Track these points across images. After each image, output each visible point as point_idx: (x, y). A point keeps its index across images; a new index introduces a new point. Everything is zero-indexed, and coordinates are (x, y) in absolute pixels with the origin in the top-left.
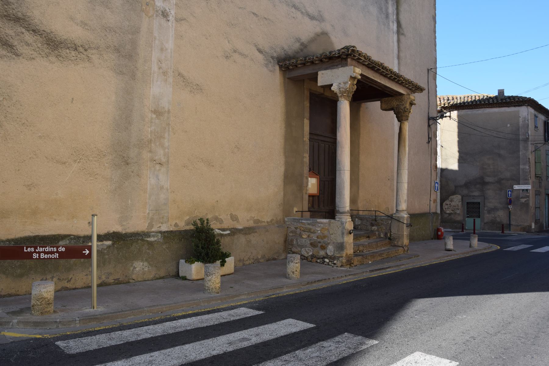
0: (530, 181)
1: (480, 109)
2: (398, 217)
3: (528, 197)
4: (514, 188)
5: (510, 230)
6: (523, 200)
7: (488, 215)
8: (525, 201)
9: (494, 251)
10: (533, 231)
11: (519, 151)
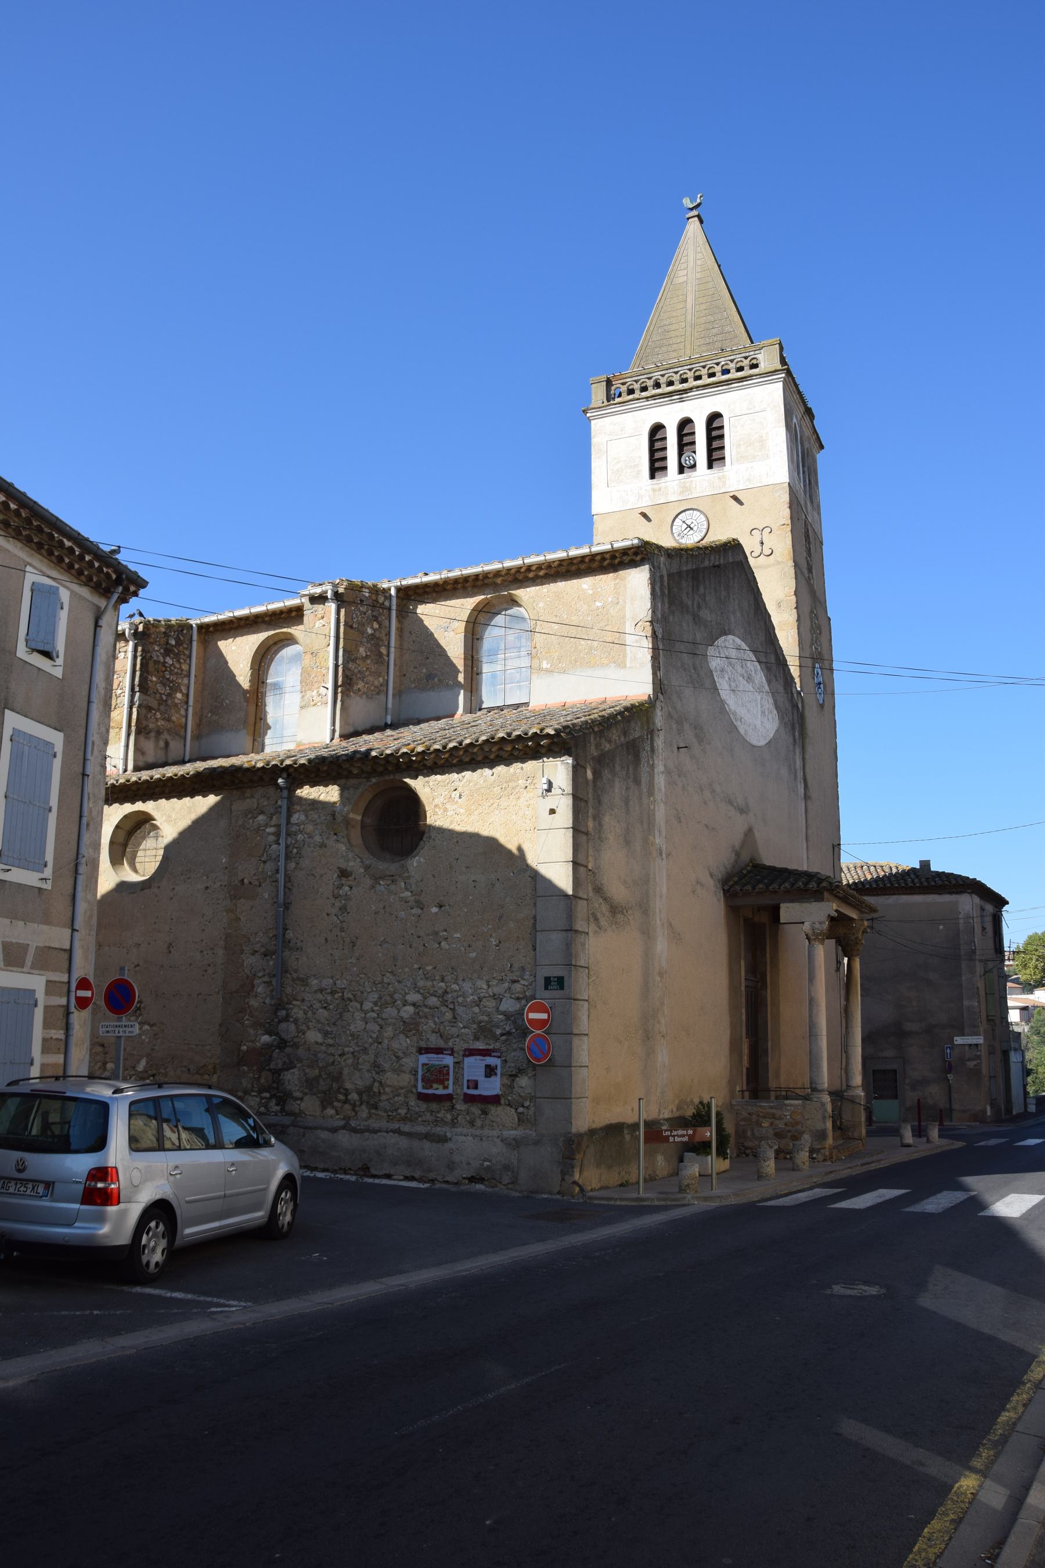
0: (981, 1029)
1: (891, 896)
2: (852, 1096)
3: (979, 1057)
4: (955, 1043)
5: (951, 1121)
6: (971, 1064)
8: (975, 1065)
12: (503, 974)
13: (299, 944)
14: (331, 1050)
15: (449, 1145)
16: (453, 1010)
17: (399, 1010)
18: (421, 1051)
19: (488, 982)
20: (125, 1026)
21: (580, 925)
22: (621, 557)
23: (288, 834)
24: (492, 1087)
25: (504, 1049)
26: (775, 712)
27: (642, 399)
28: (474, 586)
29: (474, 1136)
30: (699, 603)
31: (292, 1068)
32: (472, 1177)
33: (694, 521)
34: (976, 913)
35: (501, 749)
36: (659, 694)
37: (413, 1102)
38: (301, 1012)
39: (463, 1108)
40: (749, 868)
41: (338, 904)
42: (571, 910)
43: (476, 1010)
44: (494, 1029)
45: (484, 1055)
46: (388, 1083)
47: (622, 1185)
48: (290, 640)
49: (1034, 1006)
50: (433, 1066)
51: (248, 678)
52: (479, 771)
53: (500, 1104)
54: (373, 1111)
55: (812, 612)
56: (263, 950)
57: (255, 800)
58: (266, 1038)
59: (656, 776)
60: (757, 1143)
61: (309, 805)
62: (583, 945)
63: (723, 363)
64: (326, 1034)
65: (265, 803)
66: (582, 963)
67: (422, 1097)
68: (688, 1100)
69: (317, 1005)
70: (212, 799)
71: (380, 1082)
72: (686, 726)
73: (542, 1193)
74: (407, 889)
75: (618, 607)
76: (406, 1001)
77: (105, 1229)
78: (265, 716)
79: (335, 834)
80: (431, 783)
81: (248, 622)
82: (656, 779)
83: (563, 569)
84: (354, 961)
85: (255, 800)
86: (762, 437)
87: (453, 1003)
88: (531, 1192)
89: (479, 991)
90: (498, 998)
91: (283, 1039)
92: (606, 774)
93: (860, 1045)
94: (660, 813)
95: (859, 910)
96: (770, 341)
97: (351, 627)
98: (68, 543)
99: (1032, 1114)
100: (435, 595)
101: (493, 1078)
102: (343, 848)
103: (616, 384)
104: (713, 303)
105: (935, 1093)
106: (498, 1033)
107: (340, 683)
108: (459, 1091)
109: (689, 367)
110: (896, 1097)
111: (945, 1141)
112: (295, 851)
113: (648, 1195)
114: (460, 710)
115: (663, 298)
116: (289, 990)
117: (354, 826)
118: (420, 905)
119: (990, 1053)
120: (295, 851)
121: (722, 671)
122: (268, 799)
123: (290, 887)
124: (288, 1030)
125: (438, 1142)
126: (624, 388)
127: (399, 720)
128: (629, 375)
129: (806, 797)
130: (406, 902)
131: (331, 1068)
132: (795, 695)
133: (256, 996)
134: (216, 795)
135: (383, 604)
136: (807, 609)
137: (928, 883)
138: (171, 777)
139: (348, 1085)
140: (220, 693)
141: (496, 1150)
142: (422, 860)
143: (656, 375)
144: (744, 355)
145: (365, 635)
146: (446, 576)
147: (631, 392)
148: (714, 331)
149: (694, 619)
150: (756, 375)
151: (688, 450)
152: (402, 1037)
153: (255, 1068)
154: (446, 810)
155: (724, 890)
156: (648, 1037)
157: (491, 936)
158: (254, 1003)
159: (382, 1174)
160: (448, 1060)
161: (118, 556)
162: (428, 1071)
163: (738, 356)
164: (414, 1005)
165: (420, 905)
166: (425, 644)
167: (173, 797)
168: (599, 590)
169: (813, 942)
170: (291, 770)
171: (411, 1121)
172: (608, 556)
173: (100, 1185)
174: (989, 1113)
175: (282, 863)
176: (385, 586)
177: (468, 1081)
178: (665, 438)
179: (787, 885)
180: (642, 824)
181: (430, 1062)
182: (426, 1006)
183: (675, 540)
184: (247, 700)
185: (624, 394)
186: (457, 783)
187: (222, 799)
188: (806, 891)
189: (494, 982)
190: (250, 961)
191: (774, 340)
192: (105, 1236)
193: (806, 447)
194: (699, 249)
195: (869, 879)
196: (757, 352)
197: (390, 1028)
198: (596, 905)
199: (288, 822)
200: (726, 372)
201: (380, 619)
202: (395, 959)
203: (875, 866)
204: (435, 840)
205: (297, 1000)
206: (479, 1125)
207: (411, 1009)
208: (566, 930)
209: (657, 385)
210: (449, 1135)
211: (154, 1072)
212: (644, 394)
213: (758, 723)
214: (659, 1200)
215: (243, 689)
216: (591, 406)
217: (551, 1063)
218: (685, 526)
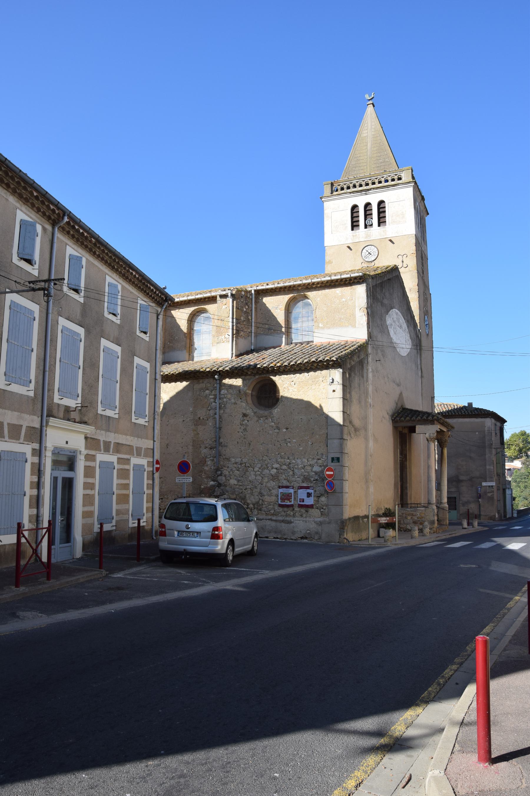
0: (494, 479)
3: (493, 492)
4: (483, 485)
6: (489, 495)
7: (462, 508)
8: (491, 495)
10: (497, 520)
11: (485, 455)
12: (314, 456)
13: (226, 444)
14: (241, 487)
15: (292, 525)
16: (293, 471)
17: (270, 471)
18: (280, 487)
19: (308, 460)
20: (187, 478)
21: (345, 437)
22: (354, 280)
23: (220, 399)
24: (310, 501)
25: (314, 486)
26: (410, 340)
27: (348, 193)
28: (289, 290)
30: (383, 297)
31: (224, 495)
32: (302, 537)
33: (372, 251)
34: (493, 429)
35: (312, 365)
36: (370, 339)
37: (276, 507)
38: (227, 472)
39: (298, 510)
40: (401, 410)
41: (242, 428)
42: (342, 431)
43: (303, 470)
44: (310, 478)
45: (306, 489)
46: (266, 500)
47: (359, 540)
48: (204, 311)
49: (514, 469)
50: (285, 493)
51: (186, 327)
52: (303, 374)
53: (313, 508)
54: (260, 512)
55: (424, 292)
56: (210, 446)
57: (204, 384)
58: (212, 483)
59: (369, 373)
60: (405, 526)
61: (229, 387)
62: (346, 445)
63: (385, 177)
64: (238, 481)
65: (209, 385)
66: (346, 452)
67: (280, 506)
68: (380, 507)
69: (234, 469)
70: (185, 384)
71: (262, 500)
72: (379, 351)
73: (331, 542)
74: (272, 422)
76: (273, 467)
77: (219, 547)
78: (194, 344)
79: (241, 399)
80: (282, 379)
81: (185, 303)
82: (369, 375)
83: (328, 284)
84: (250, 451)
86: (403, 212)
87: (293, 468)
88: (327, 542)
89: (304, 463)
90: (312, 466)
91: (220, 483)
92: (353, 374)
93: (446, 485)
94: (370, 389)
95: (447, 428)
96: (407, 168)
97: (238, 309)
98: (152, 288)
99: (515, 518)
100: (271, 293)
101: (310, 498)
102: (244, 404)
103: (336, 185)
104: (380, 147)
105: (473, 508)
106: (312, 480)
107: (234, 333)
108: (296, 503)
109: (369, 178)
110: (456, 509)
111: (480, 527)
112: (223, 405)
113: (373, 543)
115: (356, 144)
116: (222, 463)
117: (248, 396)
118: (278, 428)
119: (498, 490)
120: (223, 405)
121: (391, 325)
122: (210, 383)
123: (221, 420)
124: (221, 479)
125: (288, 523)
126: (339, 188)
127: (256, 348)
128: (342, 181)
129: (422, 377)
130: (272, 427)
131: (241, 495)
132: (418, 331)
133: (207, 466)
134: (187, 382)
135: (249, 297)
136: (422, 291)
137: (472, 413)
138: (167, 375)
139: (249, 501)
140: (173, 334)
141: (312, 526)
142: (279, 410)
143: (354, 182)
144: (395, 174)
145: (243, 312)
146: (277, 286)
147: (342, 189)
148: (381, 161)
149: (381, 304)
150: (401, 184)
151: (369, 217)
152: (271, 482)
153: (207, 495)
154: (289, 390)
155: (392, 420)
156: (367, 482)
157: (309, 441)
158: (206, 468)
159: (264, 536)
160: (292, 491)
161: (165, 290)
162: (283, 495)
163: (392, 174)
164: (276, 469)
165: (278, 428)
166: (267, 315)
167: (167, 382)
168: (344, 294)
169: (429, 442)
170: (221, 372)
171: (276, 515)
173: (216, 533)
174: (497, 517)
175: (218, 411)
176: (250, 289)
177: (300, 499)
178: (358, 212)
179: (419, 418)
180: (364, 394)
181: (284, 492)
182: (282, 469)
183: (363, 259)
184: (186, 337)
185: (339, 190)
187: (190, 383)
188: (427, 420)
189: (310, 460)
190: (204, 451)
191: (409, 167)
192: (219, 550)
193: (421, 215)
195: (444, 411)
196: (401, 172)
197: (266, 478)
198: (350, 428)
199: (220, 394)
200: (387, 181)
201: (248, 304)
202: (268, 450)
203: (447, 405)
204: (284, 402)
205: (225, 467)
206: (305, 516)
207: (275, 470)
208: (340, 439)
209: (355, 186)
210: (292, 520)
211: (162, 497)
212: (349, 191)
214: (377, 545)
215: (184, 332)
216: (324, 196)
217: (334, 492)
218: (367, 253)
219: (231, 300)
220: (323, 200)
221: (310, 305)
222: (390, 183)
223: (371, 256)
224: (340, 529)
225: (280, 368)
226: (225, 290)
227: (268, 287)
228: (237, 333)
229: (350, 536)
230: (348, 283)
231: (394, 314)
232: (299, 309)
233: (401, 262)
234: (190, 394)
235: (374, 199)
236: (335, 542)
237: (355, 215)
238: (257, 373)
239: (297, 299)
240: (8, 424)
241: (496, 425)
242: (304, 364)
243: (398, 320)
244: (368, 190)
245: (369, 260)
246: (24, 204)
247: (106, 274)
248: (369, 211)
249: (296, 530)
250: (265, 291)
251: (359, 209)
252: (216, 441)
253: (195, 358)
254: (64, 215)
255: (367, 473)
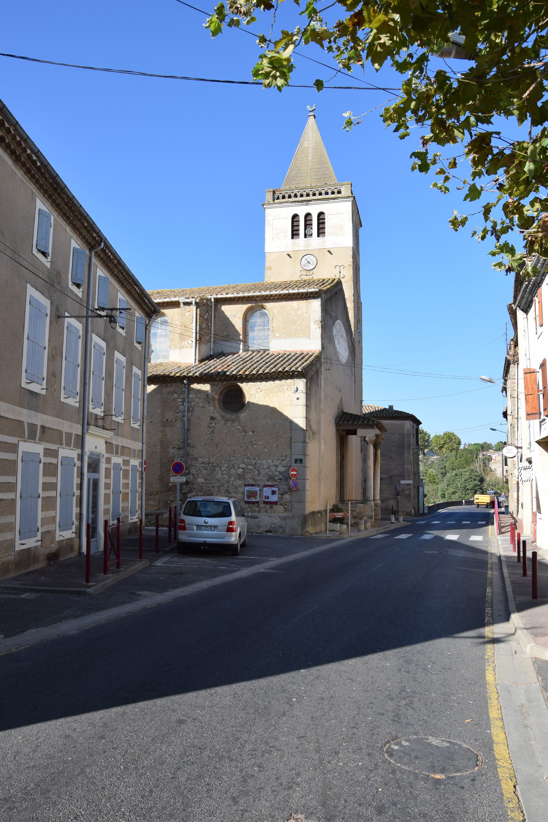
3: (410, 489)
6: (407, 492)
9: (262, 572)
14: (209, 485)
15: (258, 519)
17: (236, 470)
18: (246, 485)
21: (307, 440)
23: (188, 402)
25: (279, 485)
28: (247, 300)
29: (268, 516)
38: (195, 471)
41: (210, 430)
43: (268, 470)
44: (275, 478)
52: (269, 382)
56: (177, 447)
57: (172, 388)
64: (206, 479)
65: (177, 389)
66: (307, 454)
69: (202, 468)
73: (295, 535)
75: (308, 314)
77: (233, 539)
80: (249, 386)
83: (285, 297)
85: (172, 388)
90: (276, 466)
92: (312, 384)
96: (347, 182)
98: (147, 301)
101: (275, 495)
102: (212, 408)
103: (277, 194)
108: (261, 500)
111: (405, 522)
112: (191, 409)
114: (241, 351)
116: (189, 462)
118: (245, 431)
120: (191, 409)
122: (179, 388)
125: (254, 518)
126: (281, 196)
129: (355, 382)
134: (155, 385)
141: (277, 521)
143: (296, 192)
144: (335, 187)
147: (284, 197)
151: (309, 227)
154: (255, 396)
156: (320, 481)
160: (257, 489)
164: (242, 468)
165: (245, 431)
169: (369, 444)
172: (305, 294)
173: (231, 526)
174: (413, 512)
176: (209, 297)
178: (299, 221)
179: (361, 422)
186: (260, 386)
189: (275, 460)
190: (172, 451)
194: (314, 132)
197: (233, 477)
199: (188, 397)
200: (327, 193)
202: (234, 451)
207: (241, 470)
209: (296, 196)
213: (344, 354)
217: (297, 490)
218: (306, 262)
219: (195, 308)
220: (264, 207)
221: (267, 315)
222: (330, 196)
223: (309, 264)
224: (303, 523)
225: (248, 376)
226: (189, 298)
227: (227, 296)
228: (200, 340)
229: (310, 529)
230: (305, 297)
231: (338, 325)
232: (256, 319)
233: (339, 273)
234: (158, 397)
235: (314, 209)
236: (297, 535)
237: (295, 224)
238: (225, 379)
239: (254, 308)
240: (65, 432)
241: (413, 427)
242: (271, 374)
243: (340, 329)
244: (309, 201)
245: (308, 269)
246: (75, 232)
247: (118, 291)
248: (309, 221)
249: (261, 524)
250: (224, 300)
251: (299, 218)
252: (184, 442)
253: (152, 360)
254: (101, 241)
255: (320, 473)
